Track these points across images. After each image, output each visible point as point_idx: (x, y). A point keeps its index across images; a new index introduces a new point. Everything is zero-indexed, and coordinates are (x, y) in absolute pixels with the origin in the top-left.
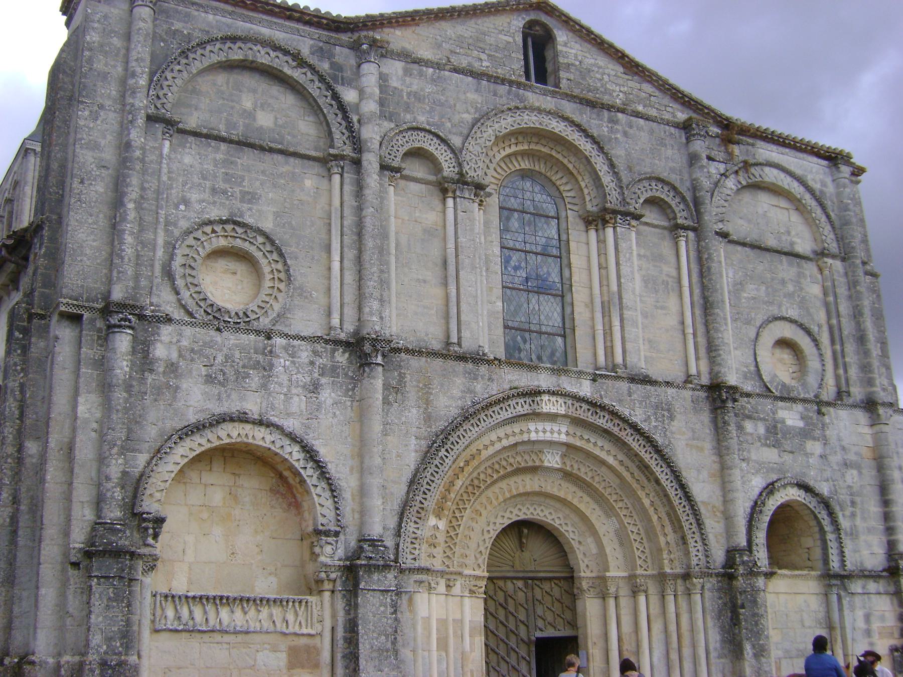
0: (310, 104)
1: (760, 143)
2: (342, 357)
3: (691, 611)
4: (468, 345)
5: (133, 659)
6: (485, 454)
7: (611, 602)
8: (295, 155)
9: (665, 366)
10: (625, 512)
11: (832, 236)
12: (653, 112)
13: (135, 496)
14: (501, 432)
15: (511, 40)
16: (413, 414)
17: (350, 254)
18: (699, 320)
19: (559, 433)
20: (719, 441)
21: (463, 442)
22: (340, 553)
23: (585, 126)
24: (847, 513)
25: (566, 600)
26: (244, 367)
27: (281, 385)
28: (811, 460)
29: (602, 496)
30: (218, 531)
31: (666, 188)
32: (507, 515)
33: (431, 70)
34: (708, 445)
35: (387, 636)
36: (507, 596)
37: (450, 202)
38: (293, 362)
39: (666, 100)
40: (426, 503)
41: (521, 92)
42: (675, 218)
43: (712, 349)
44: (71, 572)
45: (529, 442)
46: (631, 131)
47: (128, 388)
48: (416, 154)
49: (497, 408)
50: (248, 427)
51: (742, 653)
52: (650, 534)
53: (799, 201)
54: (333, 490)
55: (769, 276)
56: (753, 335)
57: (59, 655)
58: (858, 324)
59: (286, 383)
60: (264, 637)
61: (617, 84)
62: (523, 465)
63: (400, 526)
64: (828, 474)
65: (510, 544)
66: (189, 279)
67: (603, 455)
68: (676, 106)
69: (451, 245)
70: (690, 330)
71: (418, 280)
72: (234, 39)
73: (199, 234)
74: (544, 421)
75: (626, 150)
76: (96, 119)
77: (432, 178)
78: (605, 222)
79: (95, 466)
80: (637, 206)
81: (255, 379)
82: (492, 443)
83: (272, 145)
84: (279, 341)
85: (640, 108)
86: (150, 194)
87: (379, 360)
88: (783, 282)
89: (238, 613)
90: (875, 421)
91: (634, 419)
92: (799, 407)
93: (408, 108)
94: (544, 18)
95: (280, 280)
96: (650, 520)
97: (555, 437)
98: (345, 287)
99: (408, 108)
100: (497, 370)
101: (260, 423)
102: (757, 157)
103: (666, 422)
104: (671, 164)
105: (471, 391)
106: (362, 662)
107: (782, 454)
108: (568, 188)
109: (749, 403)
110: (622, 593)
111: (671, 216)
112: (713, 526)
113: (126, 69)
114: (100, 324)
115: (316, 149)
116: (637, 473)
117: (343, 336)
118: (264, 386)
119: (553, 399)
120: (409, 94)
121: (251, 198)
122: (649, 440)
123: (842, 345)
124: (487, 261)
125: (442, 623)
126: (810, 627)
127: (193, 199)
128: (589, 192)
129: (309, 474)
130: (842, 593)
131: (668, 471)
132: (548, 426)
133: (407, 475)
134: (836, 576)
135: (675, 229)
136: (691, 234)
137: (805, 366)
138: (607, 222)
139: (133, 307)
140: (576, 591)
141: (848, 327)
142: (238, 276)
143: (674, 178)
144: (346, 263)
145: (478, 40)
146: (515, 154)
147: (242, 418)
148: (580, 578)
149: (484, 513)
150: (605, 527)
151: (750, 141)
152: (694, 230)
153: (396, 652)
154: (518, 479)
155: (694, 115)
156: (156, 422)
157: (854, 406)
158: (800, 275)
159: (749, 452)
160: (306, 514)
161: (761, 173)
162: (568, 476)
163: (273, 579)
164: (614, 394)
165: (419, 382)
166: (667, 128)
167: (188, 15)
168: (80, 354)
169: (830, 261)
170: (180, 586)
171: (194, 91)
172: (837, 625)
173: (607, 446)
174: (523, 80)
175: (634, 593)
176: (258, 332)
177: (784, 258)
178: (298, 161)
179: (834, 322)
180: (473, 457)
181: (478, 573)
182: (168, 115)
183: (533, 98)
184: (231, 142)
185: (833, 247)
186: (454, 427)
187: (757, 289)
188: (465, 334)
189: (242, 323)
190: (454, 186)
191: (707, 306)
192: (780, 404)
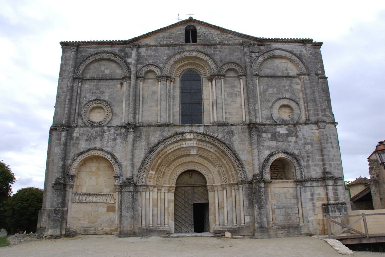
1: (272, 43)
7: (216, 193)
9: (233, 120)
11: (304, 68)
12: (231, 42)
15: (181, 33)
16: (144, 143)
24: (305, 160)
26: (96, 136)
27: (105, 139)
28: (290, 144)
30: (94, 178)
32: (183, 169)
35: (130, 203)
36: (185, 192)
37: (159, 83)
39: (236, 37)
41: (183, 47)
45: (183, 147)
50: (96, 151)
54: (120, 166)
55: (278, 85)
60: (101, 204)
61: (217, 37)
64: (298, 147)
67: (209, 149)
70: (243, 107)
71: (150, 106)
72: (97, 54)
75: (220, 56)
80: (223, 72)
83: (108, 78)
85: (226, 42)
87: (131, 130)
88: (284, 86)
93: (146, 60)
99: (146, 60)
100: (171, 128)
101: (99, 150)
102: (272, 48)
103: (231, 137)
104: (237, 57)
107: (277, 143)
109: (265, 127)
110: (219, 190)
112: (248, 168)
118: (101, 140)
120: (147, 56)
121: (102, 93)
122: (223, 143)
126: (289, 198)
127: (87, 96)
130: (301, 187)
132: (189, 142)
133: (141, 160)
135: (239, 76)
136: (244, 77)
138: (213, 79)
142: (101, 113)
143: (238, 61)
147: (95, 149)
151: (268, 43)
152: (245, 76)
159: (264, 143)
161: (273, 53)
162: (200, 156)
163: (109, 189)
165: (146, 134)
166: (236, 46)
167: (86, 51)
172: (299, 197)
173: (211, 146)
178: (116, 81)
183: (187, 48)
185: (305, 71)
187: (273, 90)
190: (160, 78)
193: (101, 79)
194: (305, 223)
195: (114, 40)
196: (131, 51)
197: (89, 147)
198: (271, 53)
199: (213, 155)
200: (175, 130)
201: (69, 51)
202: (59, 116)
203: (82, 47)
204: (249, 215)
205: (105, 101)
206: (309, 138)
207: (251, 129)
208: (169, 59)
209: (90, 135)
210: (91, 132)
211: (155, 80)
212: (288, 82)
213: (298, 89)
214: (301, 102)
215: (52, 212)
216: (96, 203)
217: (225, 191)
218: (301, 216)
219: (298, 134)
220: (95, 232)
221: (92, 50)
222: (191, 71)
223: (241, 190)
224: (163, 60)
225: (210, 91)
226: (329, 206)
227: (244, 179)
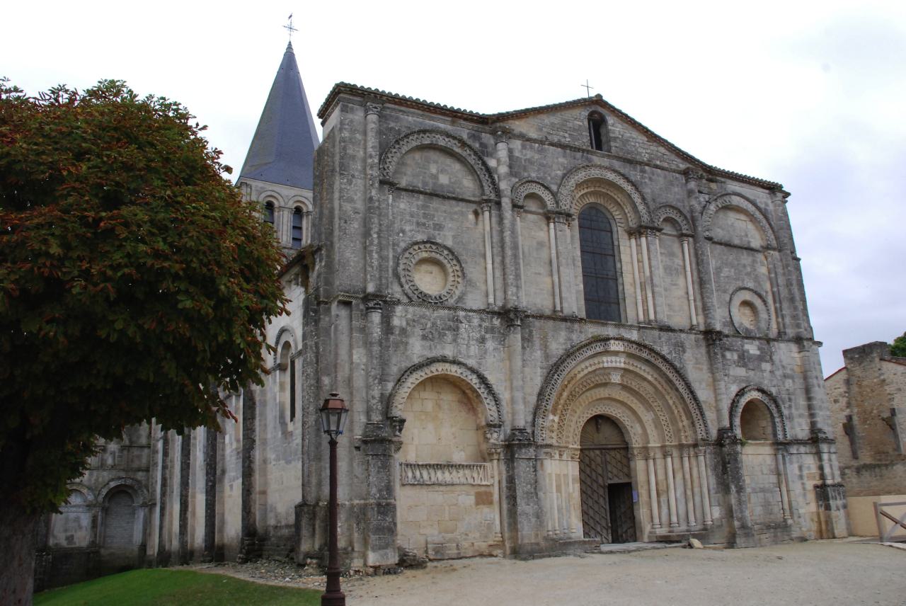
0: (468, 169)
2: (497, 322)
3: (698, 466)
4: (567, 312)
5: (393, 501)
6: (579, 376)
7: (651, 462)
8: (463, 200)
9: (679, 321)
10: (658, 408)
11: (773, 237)
12: (666, 165)
13: (388, 408)
14: (587, 363)
16: (538, 354)
17: (498, 259)
18: (697, 291)
19: (620, 362)
20: (711, 365)
21: (567, 370)
22: (502, 437)
23: (627, 176)
24: (787, 406)
25: (624, 461)
26: (443, 329)
27: (464, 339)
29: (644, 399)
30: (430, 426)
31: (675, 212)
32: (590, 412)
33: (537, 145)
34: (705, 367)
35: (531, 485)
36: (591, 460)
37: (552, 225)
38: (470, 326)
39: (673, 157)
40: (548, 407)
41: (589, 156)
42: (681, 230)
43: (706, 309)
44: (355, 452)
45: (604, 368)
46: (653, 178)
47: (380, 344)
48: (532, 196)
49: (585, 349)
51: (729, 491)
52: (674, 421)
53: (753, 216)
54: (497, 401)
56: (728, 299)
57: (351, 499)
58: (790, 290)
59: (466, 338)
60: (463, 488)
62: (600, 382)
63: (534, 420)
65: (591, 429)
66: (408, 278)
67: (645, 375)
68: (679, 160)
69: (554, 252)
71: (536, 273)
72: (424, 131)
73: (411, 250)
74: (611, 356)
76: (350, 184)
77: (541, 211)
78: (640, 234)
79: (364, 391)
81: (449, 336)
82: (583, 370)
83: (450, 195)
84: (462, 314)
85: (658, 163)
86: (384, 228)
87: (519, 323)
88: (744, 266)
89: (447, 474)
90: (802, 349)
91: (663, 353)
92: (757, 342)
93: (525, 169)
94: (600, 109)
95: (458, 276)
96: (673, 413)
97: (618, 365)
98: (496, 279)
99: (525, 169)
101: (454, 362)
104: (678, 197)
105: (570, 339)
106: (518, 500)
108: (617, 213)
110: (657, 456)
111: (678, 228)
112: (710, 415)
113: (365, 153)
114: (362, 307)
115: (474, 196)
116: (665, 385)
117: (496, 309)
118: (455, 341)
119: (617, 342)
120: (525, 160)
121: (439, 227)
123: (780, 303)
124: (574, 260)
125: (558, 476)
128: (631, 215)
129: (482, 391)
131: (683, 383)
132: (613, 358)
133: (537, 390)
134: (781, 444)
135: (681, 236)
136: (691, 239)
137: (758, 317)
139: (382, 296)
140: (630, 456)
141: (784, 293)
142: (433, 275)
143: (679, 205)
144: (496, 265)
145: (563, 125)
146: (586, 194)
147: (444, 360)
148: (633, 448)
149: (578, 411)
150: (647, 417)
151: (723, 180)
152: (692, 236)
153: (537, 494)
154: (596, 390)
155: (691, 166)
156: (396, 364)
157: (789, 341)
158: (754, 261)
159: (729, 370)
160: (480, 415)
162: (624, 387)
163: (463, 453)
164: (651, 338)
167: (397, 118)
168: (351, 325)
169: (772, 252)
170: (412, 458)
171: (403, 164)
172: (782, 472)
173: (648, 369)
174: (590, 148)
175: (665, 457)
176: (449, 308)
177: (744, 251)
178: (464, 204)
179: (775, 289)
180: (572, 378)
181: (575, 446)
182: (391, 180)
183: (596, 160)
184: (426, 194)
185: (774, 243)
186: (562, 360)
187: (730, 271)
188: (565, 305)
189: (438, 303)
191: (702, 283)
192: (746, 341)
193: (433, 195)
194: (796, 518)
195: (446, 106)
196: (492, 142)
197: (430, 355)
198: (727, 198)
199: (650, 389)
200: (591, 330)
201: (357, 109)
202: (353, 270)
203: (389, 108)
204: (719, 505)
205: (446, 248)
206: (789, 367)
207: (711, 342)
208: (568, 173)
209: (429, 325)
210: (432, 320)
211: (540, 216)
212: (750, 259)
213: (764, 274)
214: (770, 300)
215: (373, 509)
216: (453, 485)
217: (669, 459)
218: (786, 506)
219: (774, 357)
220: (459, 553)
221: (412, 120)
222: (597, 210)
223: (702, 458)
224: (556, 175)
225: (635, 259)
226: (829, 489)
227: (705, 436)
